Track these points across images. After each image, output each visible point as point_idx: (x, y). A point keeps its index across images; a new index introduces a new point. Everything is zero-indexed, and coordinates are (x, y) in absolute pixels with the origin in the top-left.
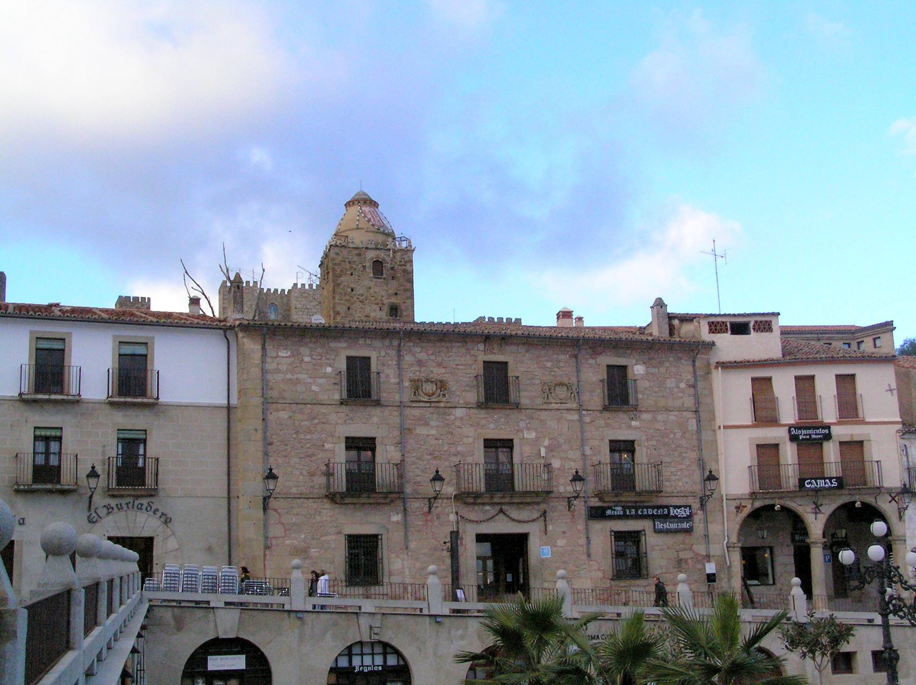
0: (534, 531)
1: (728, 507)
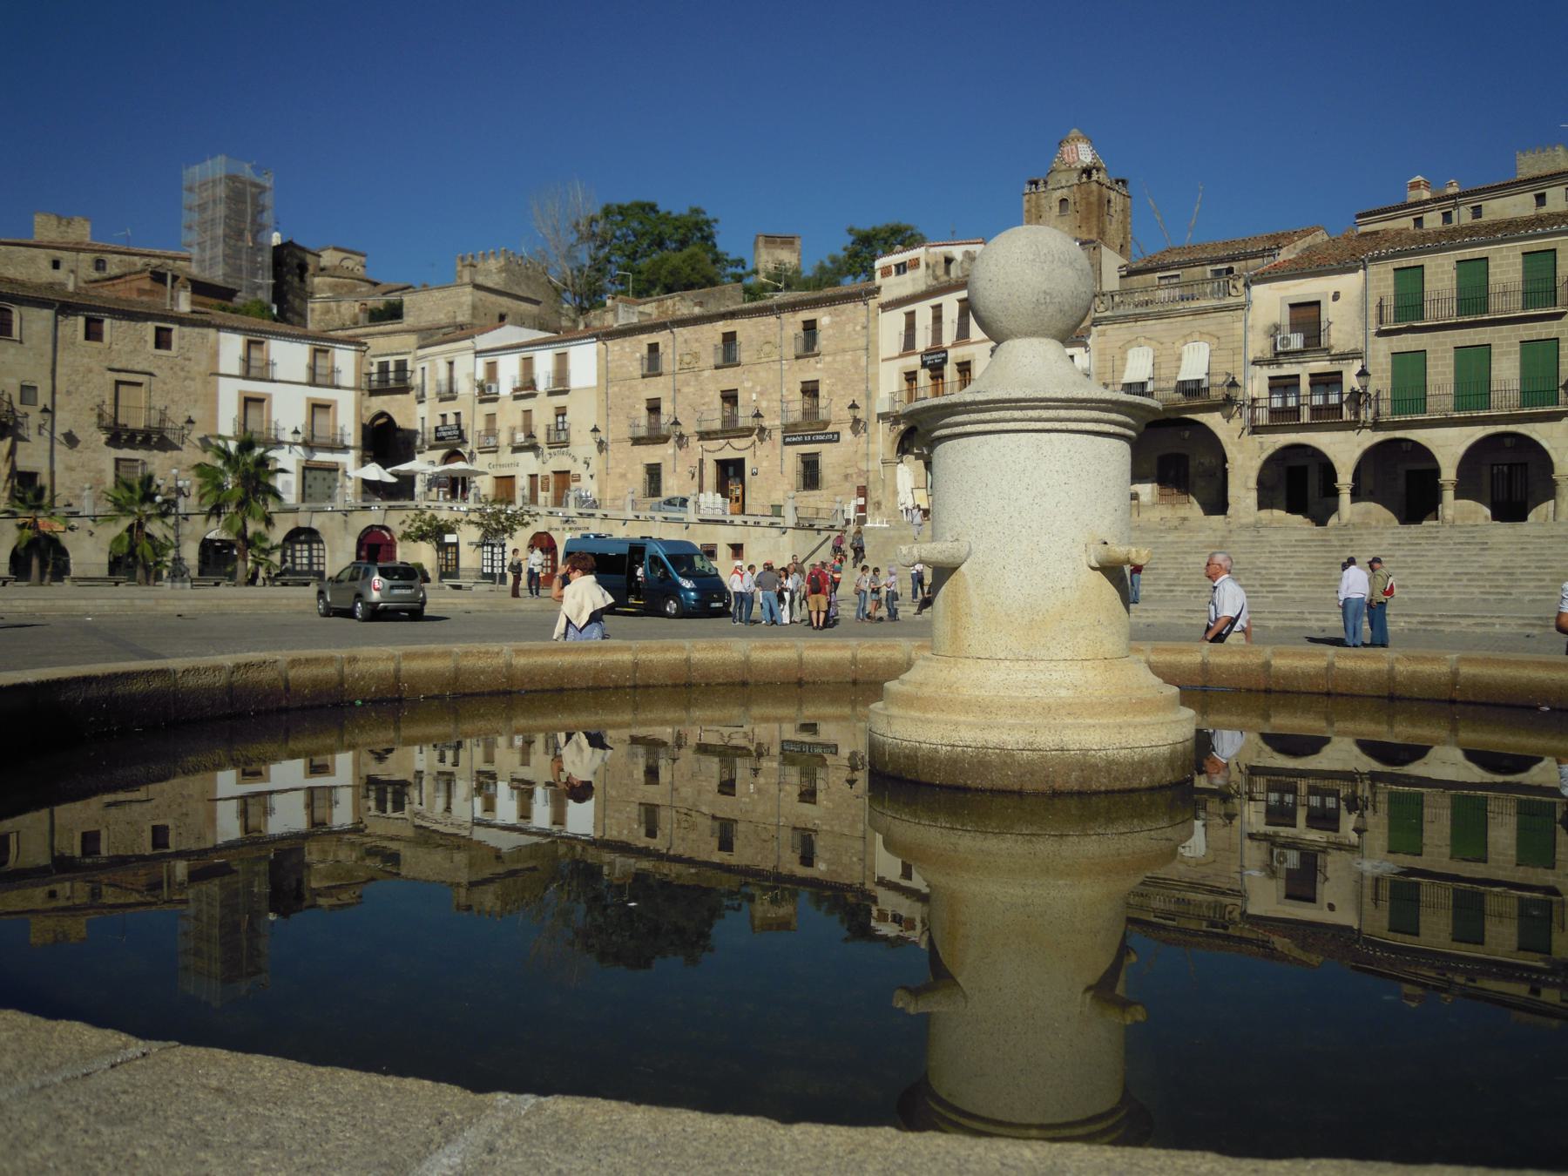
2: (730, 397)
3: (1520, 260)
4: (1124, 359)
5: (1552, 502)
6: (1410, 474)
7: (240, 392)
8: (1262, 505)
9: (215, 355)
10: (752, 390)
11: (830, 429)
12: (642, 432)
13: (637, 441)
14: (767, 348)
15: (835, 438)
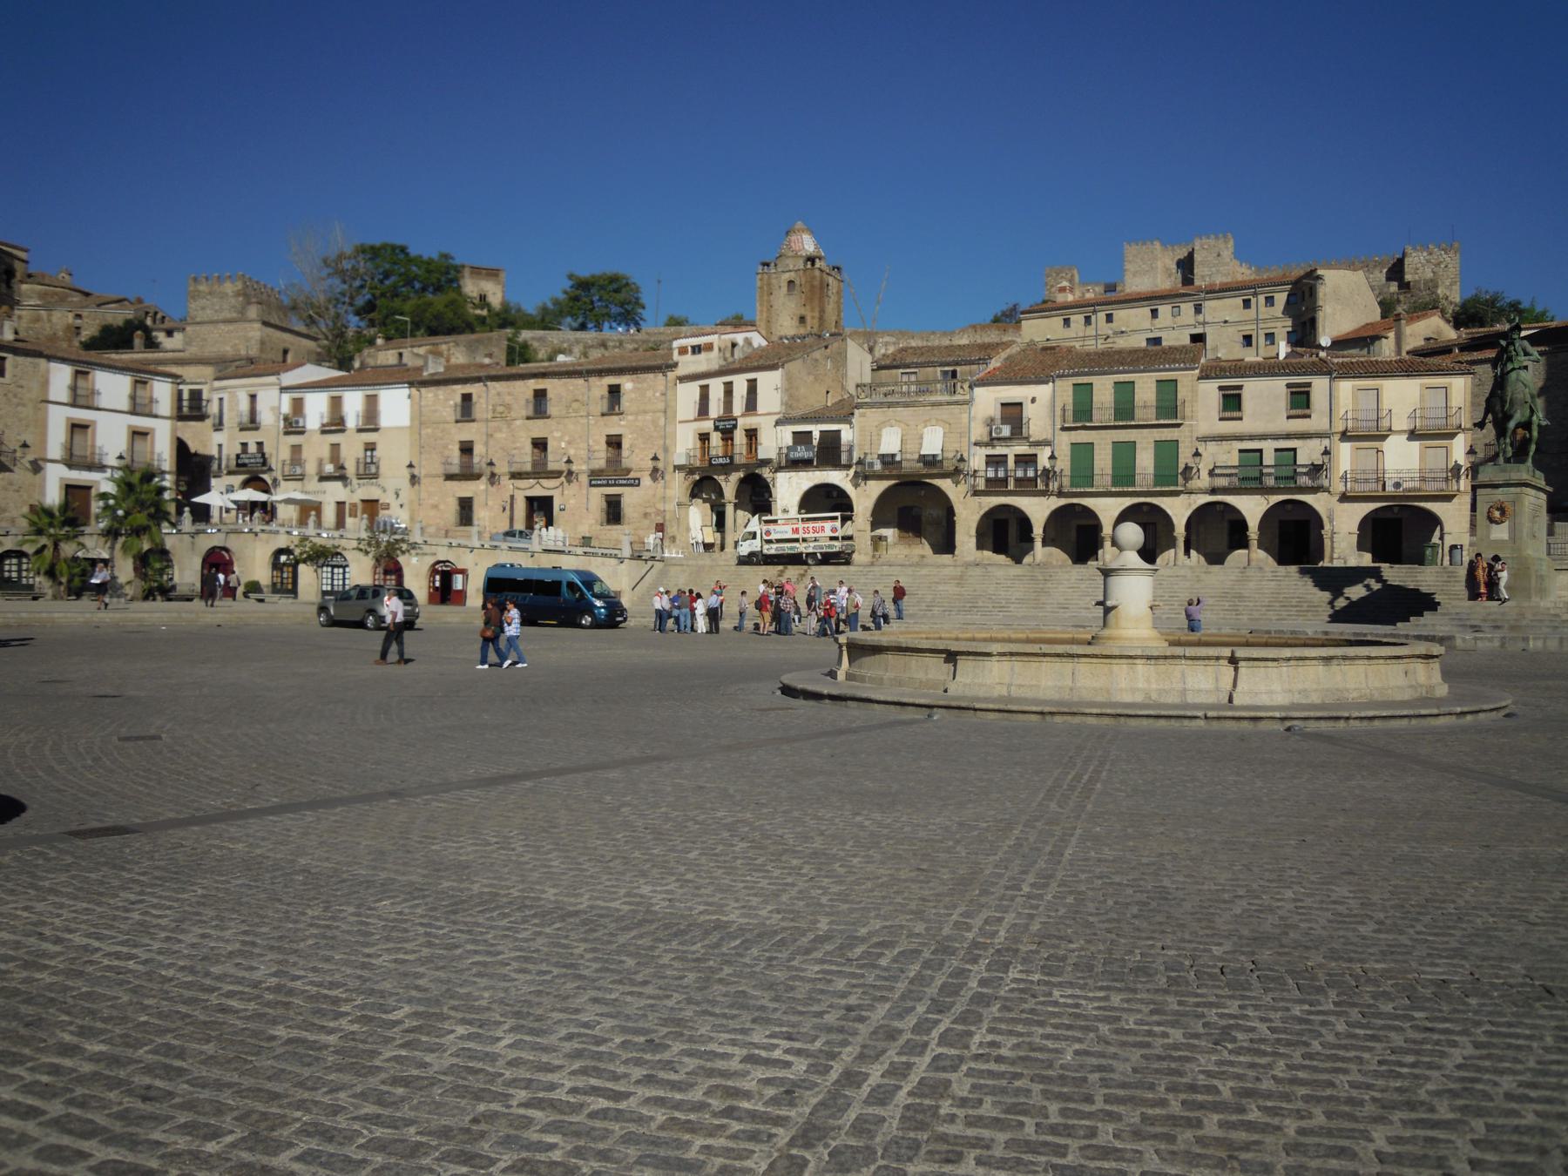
0: (556, 494)
1: (1368, 461)
2: (540, 445)
3: (1154, 385)
4: (879, 435)
5: (1172, 551)
6: (1080, 528)
7: (68, 419)
8: (980, 546)
9: (45, 384)
10: (561, 439)
11: (632, 475)
12: (455, 470)
13: (450, 477)
14: (575, 405)
15: (636, 483)
